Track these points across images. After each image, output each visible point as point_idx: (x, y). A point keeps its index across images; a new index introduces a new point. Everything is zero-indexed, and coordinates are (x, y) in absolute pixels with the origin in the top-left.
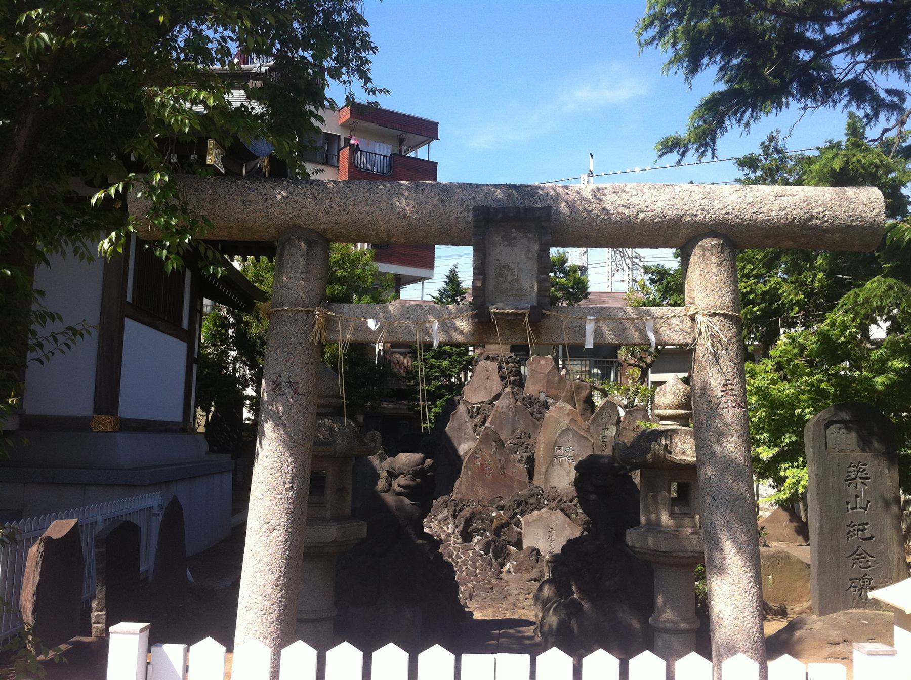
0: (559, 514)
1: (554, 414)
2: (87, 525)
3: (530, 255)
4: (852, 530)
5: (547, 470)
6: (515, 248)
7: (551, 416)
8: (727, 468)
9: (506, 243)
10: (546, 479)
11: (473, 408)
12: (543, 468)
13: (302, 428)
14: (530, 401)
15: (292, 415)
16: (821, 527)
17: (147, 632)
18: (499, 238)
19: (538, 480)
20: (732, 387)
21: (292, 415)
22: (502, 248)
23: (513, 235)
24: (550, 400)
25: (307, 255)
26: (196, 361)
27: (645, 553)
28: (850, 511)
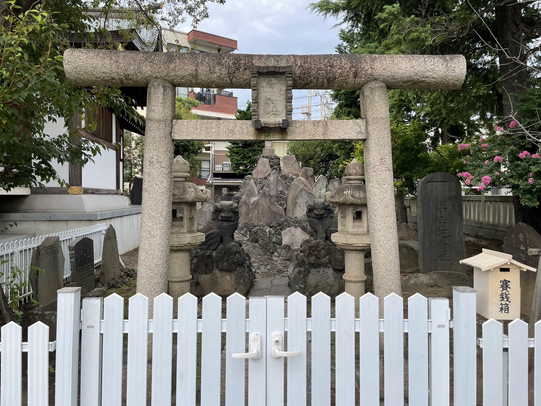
0: (299, 229)
1: (296, 183)
2: (67, 240)
3: (282, 93)
4: (439, 233)
5: (293, 209)
6: (274, 89)
7: (295, 184)
8: (382, 201)
9: (269, 86)
10: (293, 214)
11: (257, 181)
12: (291, 209)
13: (166, 186)
14: (285, 177)
15: (160, 179)
16: (424, 232)
17: (79, 293)
18: (265, 83)
19: (289, 214)
20: (386, 160)
21: (160, 179)
22: (267, 89)
23: (272, 82)
24: (294, 177)
25: (163, 93)
26: (122, 160)
27: (340, 245)
28: (438, 224)
